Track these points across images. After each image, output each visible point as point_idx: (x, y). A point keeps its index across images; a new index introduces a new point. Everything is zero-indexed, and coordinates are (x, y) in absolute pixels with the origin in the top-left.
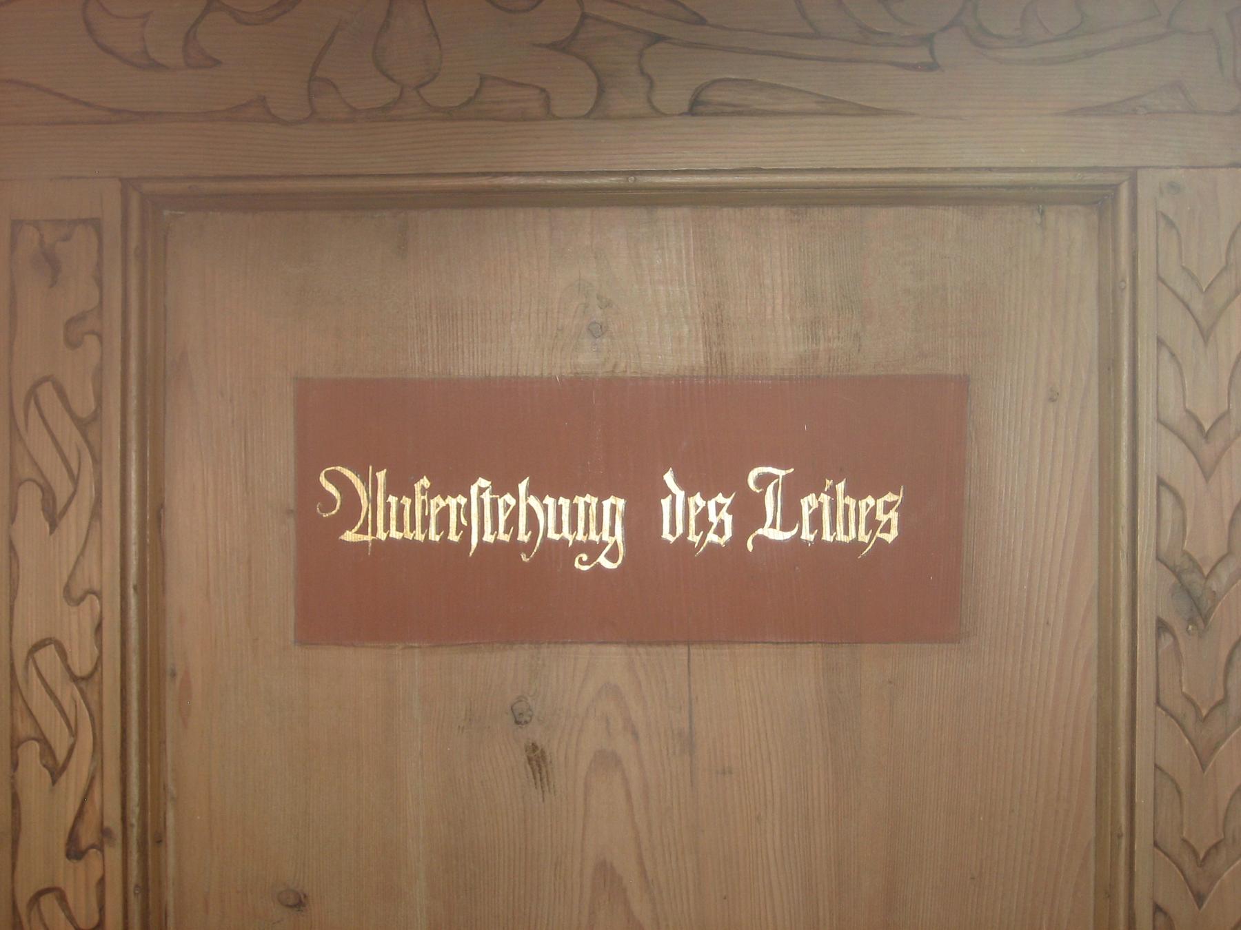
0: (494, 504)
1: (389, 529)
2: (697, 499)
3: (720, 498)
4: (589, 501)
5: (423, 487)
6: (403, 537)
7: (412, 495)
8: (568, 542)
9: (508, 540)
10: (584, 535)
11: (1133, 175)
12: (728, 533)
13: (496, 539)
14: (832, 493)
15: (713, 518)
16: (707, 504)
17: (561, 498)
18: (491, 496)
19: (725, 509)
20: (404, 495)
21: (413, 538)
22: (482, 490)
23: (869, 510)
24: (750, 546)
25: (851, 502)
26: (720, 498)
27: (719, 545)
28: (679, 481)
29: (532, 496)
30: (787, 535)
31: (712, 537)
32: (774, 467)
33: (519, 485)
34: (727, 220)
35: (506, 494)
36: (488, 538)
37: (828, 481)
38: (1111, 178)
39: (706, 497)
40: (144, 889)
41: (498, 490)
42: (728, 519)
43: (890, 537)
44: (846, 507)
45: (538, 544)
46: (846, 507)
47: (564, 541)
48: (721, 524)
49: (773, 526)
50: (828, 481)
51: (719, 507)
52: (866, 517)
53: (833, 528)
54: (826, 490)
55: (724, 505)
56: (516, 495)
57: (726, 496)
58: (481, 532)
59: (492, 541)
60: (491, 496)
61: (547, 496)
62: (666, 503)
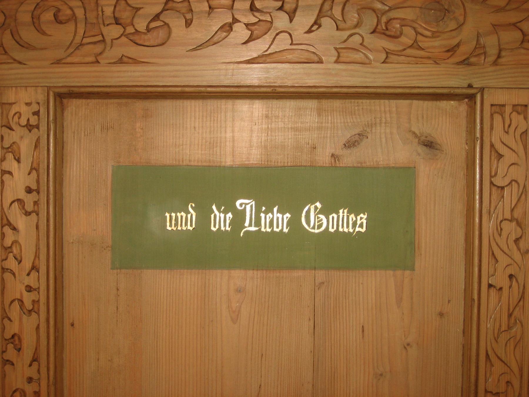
0: (348, 217)
1: (187, 226)
2: (352, 216)
7: (187, 212)
11: (482, 90)
21: (348, 231)
23: (353, 221)
25: (280, 216)
26: (362, 215)
27: (361, 232)
29: (278, 213)
30: (257, 229)
31: (358, 229)
34: (508, 89)
35: (290, 214)
37: (263, 207)
38: (51, 94)
41: (349, 212)
43: (363, 230)
44: (278, 218)
46: (278, 218)
47: (344, 232)
49: (250, 225)
50: (263, 207)
51: (361, 218)
54: (222, 210)
55: (363, 218)
56: (273, 213)
57: (364, 214)
59: (265, 231)
61: (288, 213)
62: (212, 216)
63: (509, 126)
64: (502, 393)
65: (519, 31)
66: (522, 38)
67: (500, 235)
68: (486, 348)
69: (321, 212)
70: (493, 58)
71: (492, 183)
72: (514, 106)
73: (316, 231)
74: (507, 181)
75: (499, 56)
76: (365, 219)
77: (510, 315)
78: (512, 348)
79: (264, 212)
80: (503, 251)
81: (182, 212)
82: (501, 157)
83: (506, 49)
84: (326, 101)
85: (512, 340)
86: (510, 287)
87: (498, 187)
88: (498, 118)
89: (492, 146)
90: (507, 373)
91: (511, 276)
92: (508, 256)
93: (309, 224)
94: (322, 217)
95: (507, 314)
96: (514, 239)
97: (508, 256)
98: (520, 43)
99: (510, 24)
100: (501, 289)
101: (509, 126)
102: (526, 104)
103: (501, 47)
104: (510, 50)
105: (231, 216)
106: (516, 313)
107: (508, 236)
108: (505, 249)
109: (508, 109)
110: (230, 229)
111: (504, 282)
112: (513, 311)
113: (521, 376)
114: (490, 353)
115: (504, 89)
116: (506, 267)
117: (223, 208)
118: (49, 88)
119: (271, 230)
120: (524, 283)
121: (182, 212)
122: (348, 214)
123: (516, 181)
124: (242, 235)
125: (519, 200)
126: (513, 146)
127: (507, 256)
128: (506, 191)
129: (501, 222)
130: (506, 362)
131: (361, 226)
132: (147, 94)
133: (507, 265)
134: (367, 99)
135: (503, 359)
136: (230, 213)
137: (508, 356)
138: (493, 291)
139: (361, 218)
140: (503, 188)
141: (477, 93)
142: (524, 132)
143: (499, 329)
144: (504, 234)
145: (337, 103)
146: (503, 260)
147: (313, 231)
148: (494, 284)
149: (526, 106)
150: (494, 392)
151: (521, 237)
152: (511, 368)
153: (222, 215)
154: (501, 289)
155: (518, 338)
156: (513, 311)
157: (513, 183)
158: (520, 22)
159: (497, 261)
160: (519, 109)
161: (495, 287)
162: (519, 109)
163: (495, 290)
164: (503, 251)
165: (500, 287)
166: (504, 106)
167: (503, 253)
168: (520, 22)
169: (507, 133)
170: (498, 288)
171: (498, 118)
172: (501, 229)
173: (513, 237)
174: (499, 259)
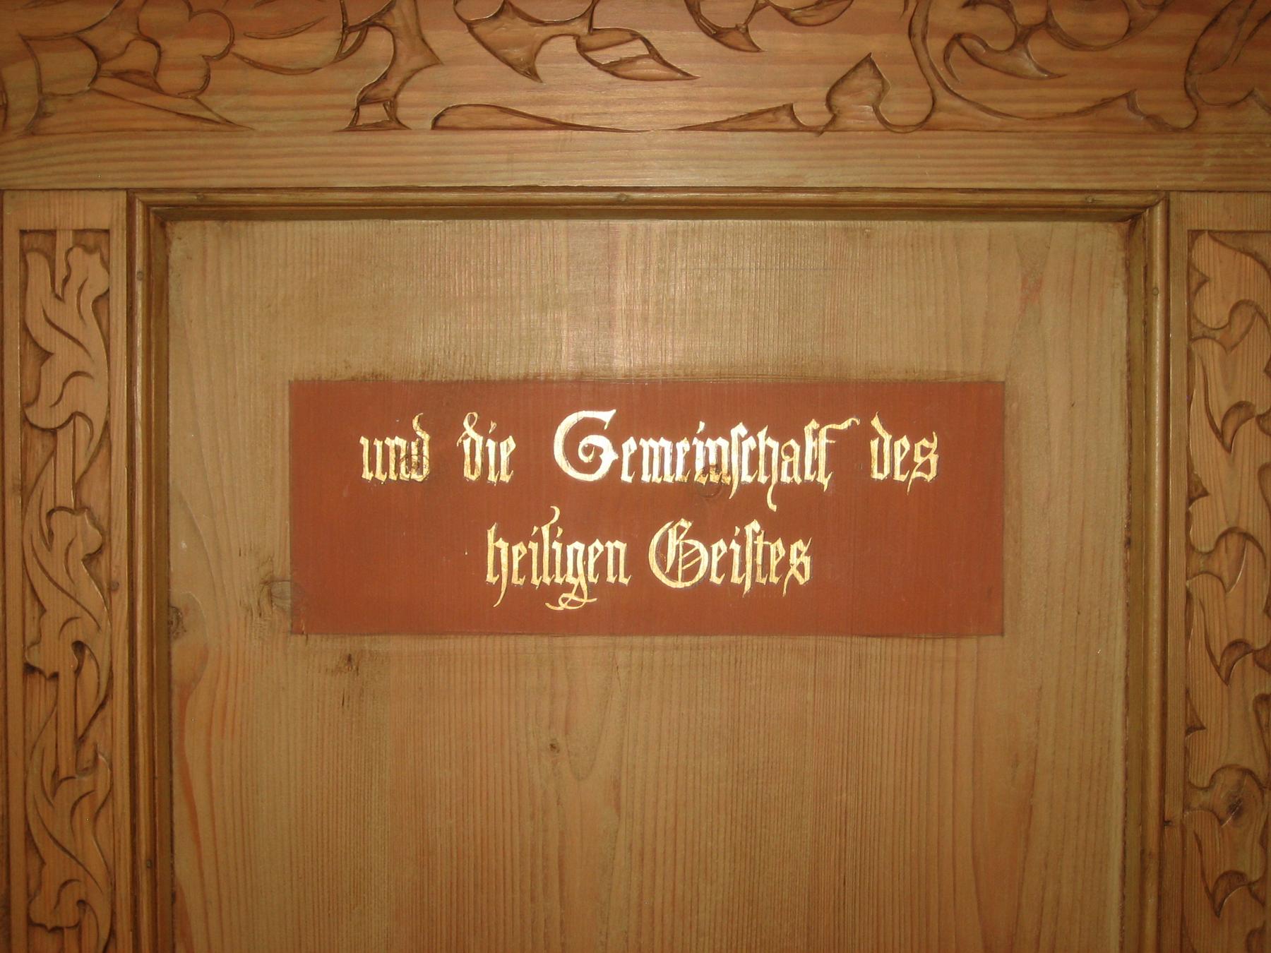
3: (925, 443)
4: (617, 547)
5: (753, 531)
6: (374, 478)
7: (728, 438)
8: (823, 486)
9: (683, 520)
10: (659, 477)
11: (1165, 196)
12: (426, 471)
13: (662, 480)
14: (539, 538)
15: (919, 459)
16: (384, 443)
17: (388, 439)
18: (828, 441)
19: (933, 451)
20: (633, 436)
22: (755, 535)
24: (773, 507)
28: (886, 427)
32: (586, 410)
33: (489, 531)
36: (786, 479)
38: (139, 208)
39: (913, 441)
40: (152, 864)
42: (933, 459)
45: (732, 495)
48: (927, 464)
51: (799, 553)
52: (718, 562)
53: (651, 471)
57: (931, 440)
58: (740, 476)
60: (828, 441)
62: (874, 444)
63: (66, 281)
64: (68, 928)
65: (88, 51)
66: (95, 67)
67: (50, 548)
68: (26, 818)
69: (692, 534)
70: (26, 117)
71: (25, 420)
72: (77, 232)
73: (679, 585)
74: (61, 415)
75: (41, 114)
76: (806, 554)
77: (80, 740)
78: (87, 819)
79: (559, 541)
80: (56, 584)
81: (397, 438)
82: (47, 358)
83: (54, 95)
84: (358, 222)
85: (85, 801)
86: (78, 671)
87: (43, 430)
88: (38, 264)
89: (25, 328)
90: (78, 881)
91: (79, 646)
92: (68, 595)
93: (662, 565)
94: (698, 545)
95: (70, 739)
96: (81, 556)
97: (68, 595)
98: (90, 80)
99: (66, 34)
100: (55, 676)
101: (66, 281)
102: (107, 228)
103: (46, 90)
104: (66, 98)
105: (513, 446)
106: (92, 734)
107: (67, 550)
108: (62, 580)
109: (64, 240)
110: (631, 478)
111: (64, 661)
112: (86, 730)
113: (114, 886)
114: (34, 831)
115: (52, 193)
116: (64, 624)
117: (493, 425)
118: (131, 194)
119: (497, 582)
120: (111, 663)
121: (397, 438)
122: (767, 543)
123: (82, 415)
124: (595, 599)
125: (90, 463)
126: (74, 328)
127: (65, 596)
128: (64, 437)
129: (50, 514)
130: (73, 853)
131: (926, 467)
132: (228, 209)
133: (65, 619)
134: (703, 218)
135: (68, 847)
136: (597, 540)
137: (79, 840)
138: (37, 683)
139: (925, 451)
140: (53, 432)
141: (1151, 207)
142: (101, 296)
143: (56, 772)
144: (59, 544)
145: (902, 228)
146: (58, 607)
147: (673, 585)
148: (42, 667)
149: (107, 232)
150: (49, 926)
151: (100, 551)
152: (88, 869)
153: (491, 444)
154: (55, 676)
155: (101, 796)
156: (86, 730)
157: (79, 420)
158: (91, 28)
159: (43, 610)
160: (90, 240)
161: (41, 672)
162: (90, 240)
163: (43, 680)
164: (56, 584)
165: (52, 671)
166: (52, 233)
167: (56, 588)
168: (91, 28)
169: (60, 298)
170: (48, 675)
171: (38, 264)
172: (51, 533)
173: (80, 550)
174: (46, 607)
